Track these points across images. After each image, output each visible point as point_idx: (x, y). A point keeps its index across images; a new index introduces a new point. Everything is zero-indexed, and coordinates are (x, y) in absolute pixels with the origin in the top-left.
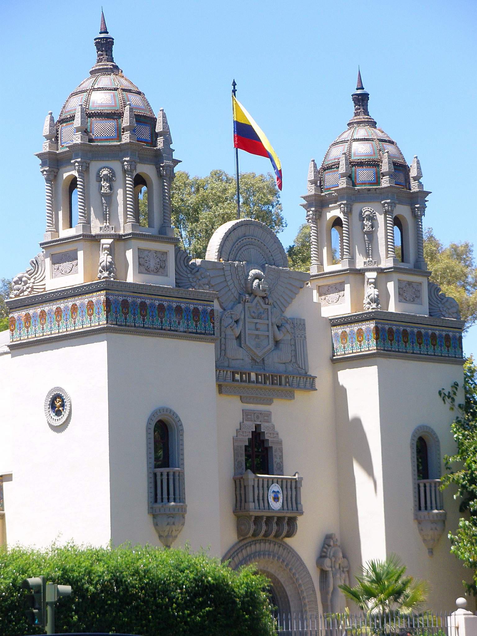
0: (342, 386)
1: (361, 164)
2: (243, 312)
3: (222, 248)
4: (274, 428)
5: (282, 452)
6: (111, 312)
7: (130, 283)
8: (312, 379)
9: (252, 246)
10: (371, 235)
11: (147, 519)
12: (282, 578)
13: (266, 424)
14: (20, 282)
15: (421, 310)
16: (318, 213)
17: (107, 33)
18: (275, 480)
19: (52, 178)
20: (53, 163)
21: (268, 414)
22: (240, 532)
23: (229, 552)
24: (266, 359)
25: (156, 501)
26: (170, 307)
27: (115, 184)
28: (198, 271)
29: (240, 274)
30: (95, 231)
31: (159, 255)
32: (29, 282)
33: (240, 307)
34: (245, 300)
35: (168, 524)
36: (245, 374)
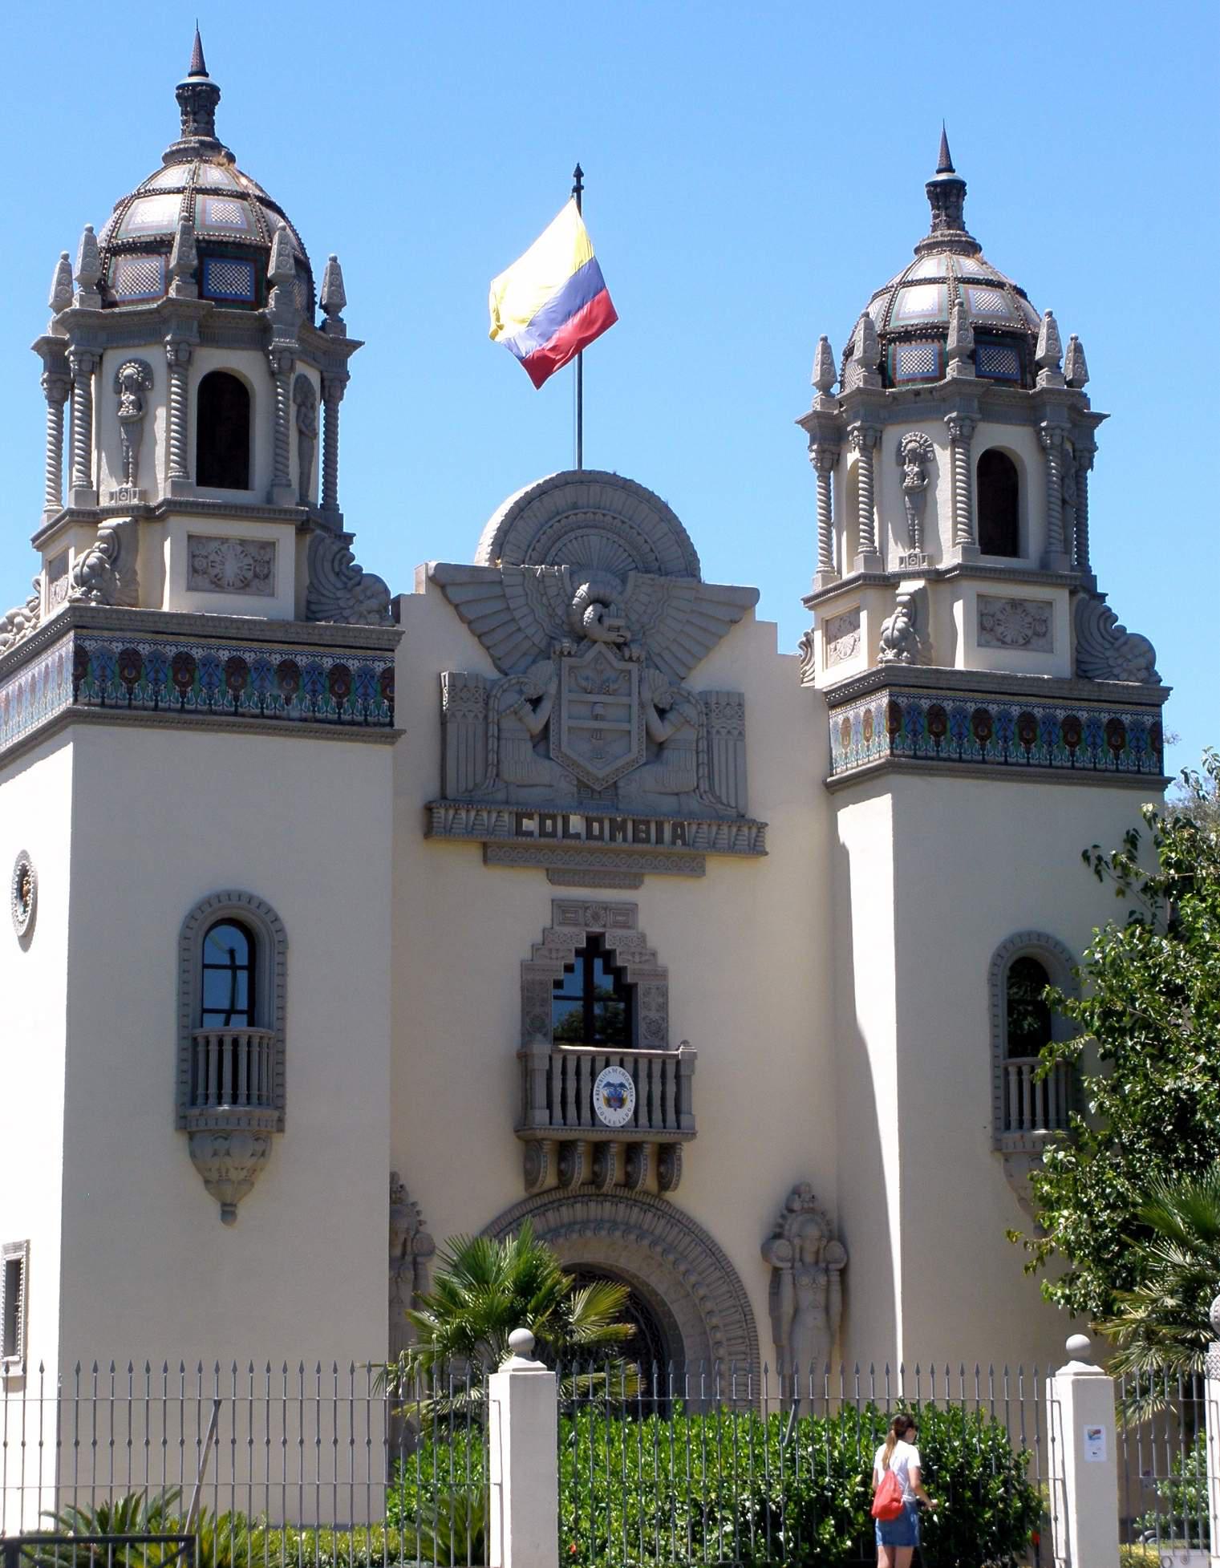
0: (843, 847)
1: (907, 336)
2: (555, 680)
4: (644, 941)
5: (664, 993)
8: (754, 830)
9: (593, 531)
10: (920, 497)
11: (176, 1144)
12: (660, 1282)
13: (620, 932)
15: (1050, 662)
16: (828, 455)
17: (206, 75)
18: (615, 1059)
21: (628, 912)
22: (530, 1178)
23: (494, 1223)
24: (621, 784)
25: (193, 1103)
26: (262, 666)
27: (153, 396)
29: (553, 591)
30: (893, 566)
31: (252, 550)
32: (27, 625)
33: (546, 667)
35: (215, 1154)
36: (554, 818)
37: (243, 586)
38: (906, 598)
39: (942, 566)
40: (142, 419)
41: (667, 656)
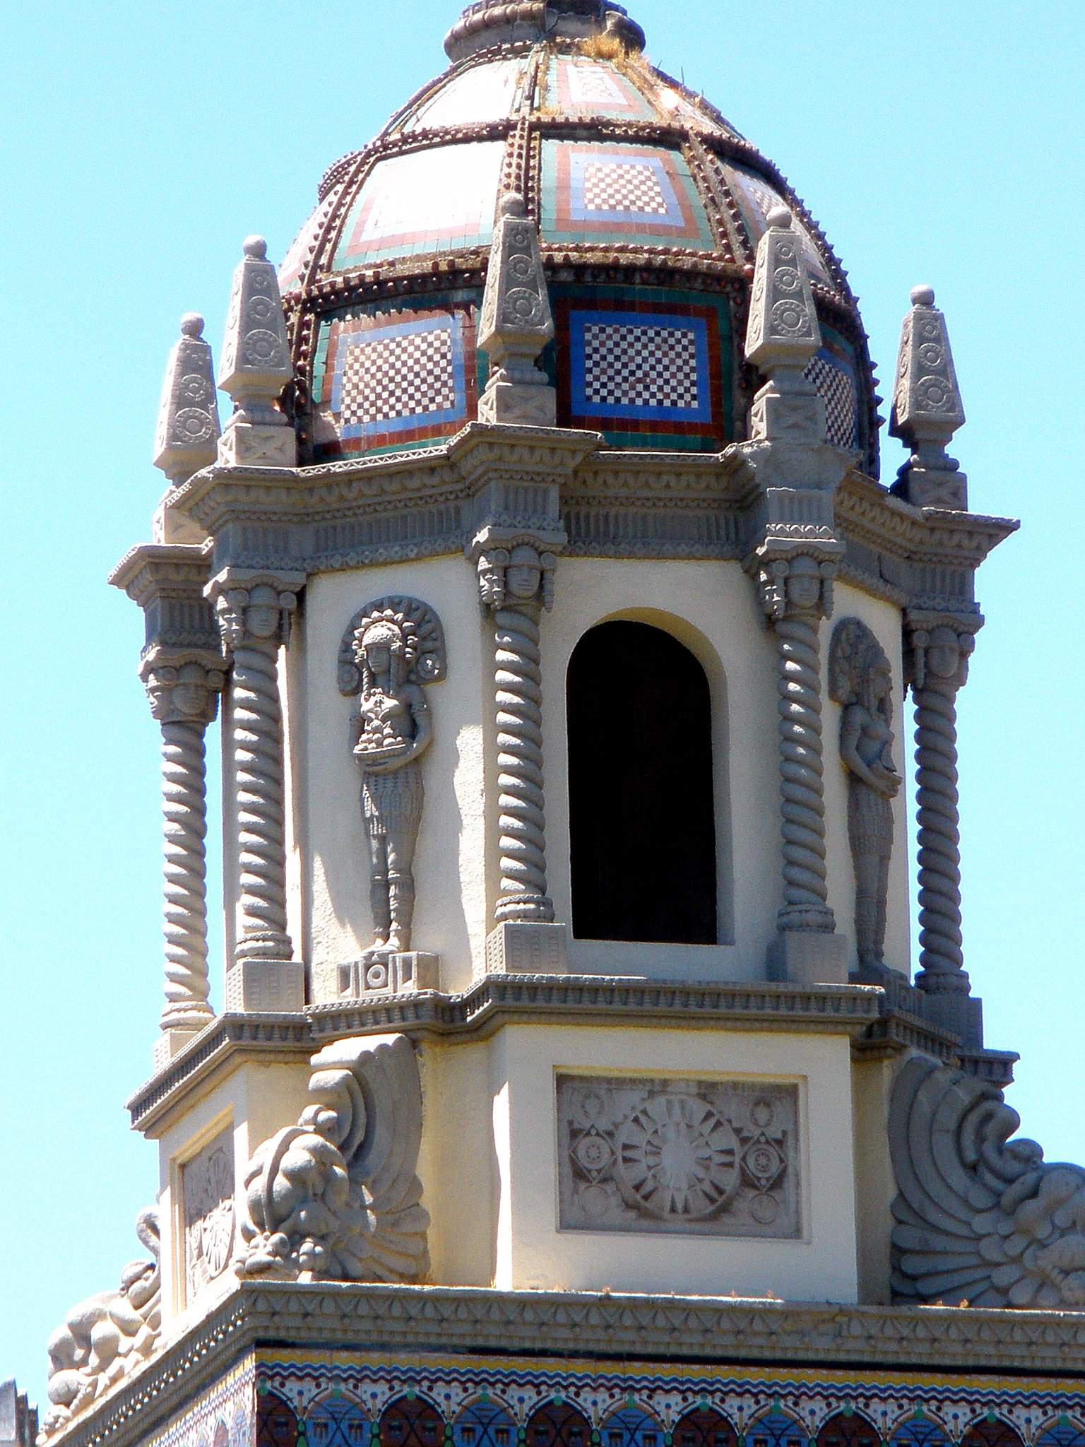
7: (502, 1298)
10: (402, 785)
14: (79, 1353)
28: (1034, 1193)
31: (734, 1109)
32: (125, 1343)
37: (713, 1213)
38: (334, 1076)
39: (459, 990)
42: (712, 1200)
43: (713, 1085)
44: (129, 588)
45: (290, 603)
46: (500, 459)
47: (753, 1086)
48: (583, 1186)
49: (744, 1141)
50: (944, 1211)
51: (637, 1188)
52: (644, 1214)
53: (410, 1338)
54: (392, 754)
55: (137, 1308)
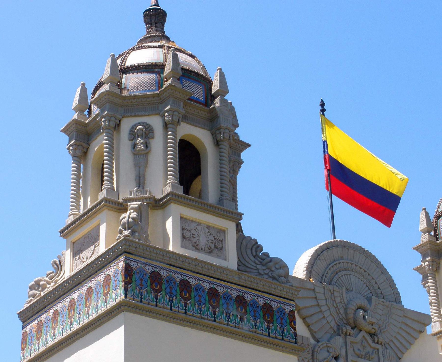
2: (344, 347)
3: (312, 267)
6: (134, 285)
19: (78, 153)
20: (81, 136)
26: (227, 296)
34: (346, 333)
37: (210, 252)
40: (147, 154)
41: (391, 344)
42: (209, 249)
43: (209, 226)
44: (65, 132)
45: (118, 122)
46: (173, 93)
47: (217, 229)
48: (185, 240)
49: (215, 239)
50: (249, 263)
51: (195, 243)
52: (196, 249)
53: (157, 258)
54: (143, 150)
55: (51, 280)
